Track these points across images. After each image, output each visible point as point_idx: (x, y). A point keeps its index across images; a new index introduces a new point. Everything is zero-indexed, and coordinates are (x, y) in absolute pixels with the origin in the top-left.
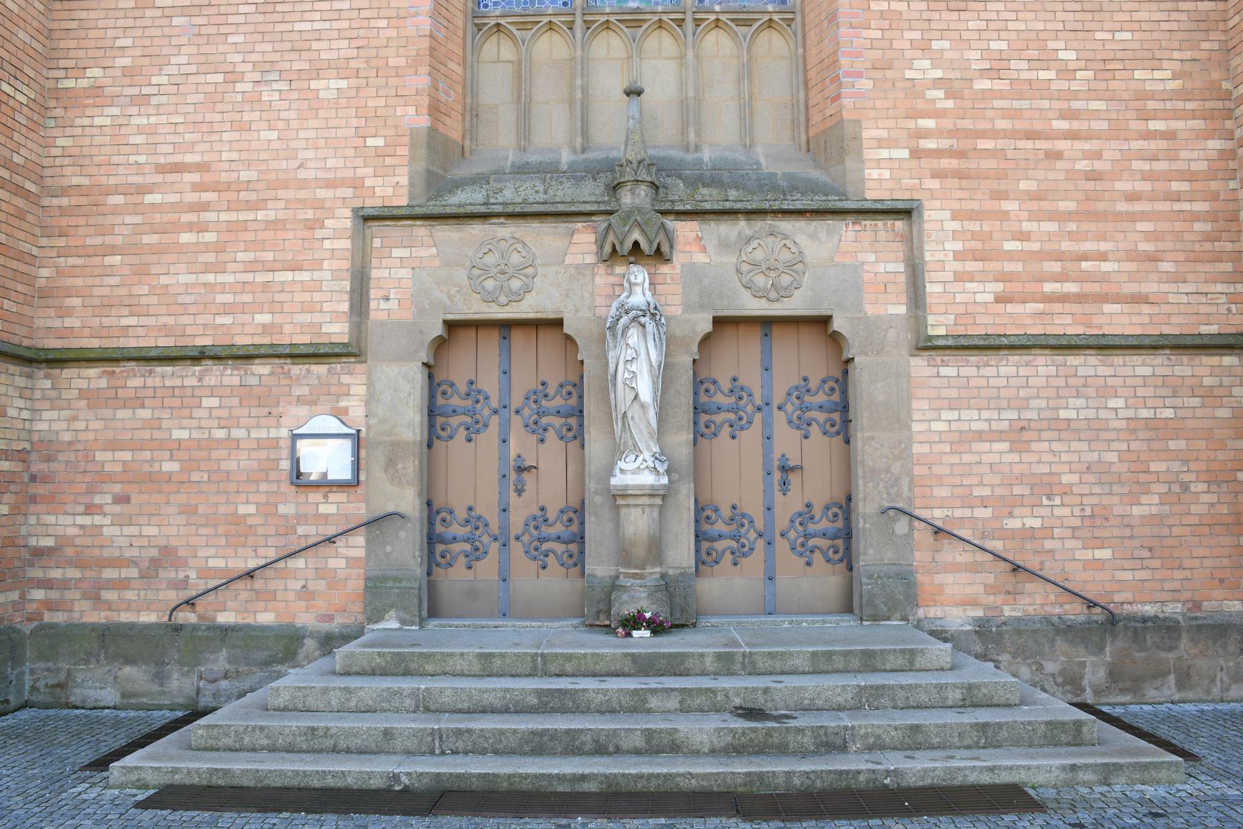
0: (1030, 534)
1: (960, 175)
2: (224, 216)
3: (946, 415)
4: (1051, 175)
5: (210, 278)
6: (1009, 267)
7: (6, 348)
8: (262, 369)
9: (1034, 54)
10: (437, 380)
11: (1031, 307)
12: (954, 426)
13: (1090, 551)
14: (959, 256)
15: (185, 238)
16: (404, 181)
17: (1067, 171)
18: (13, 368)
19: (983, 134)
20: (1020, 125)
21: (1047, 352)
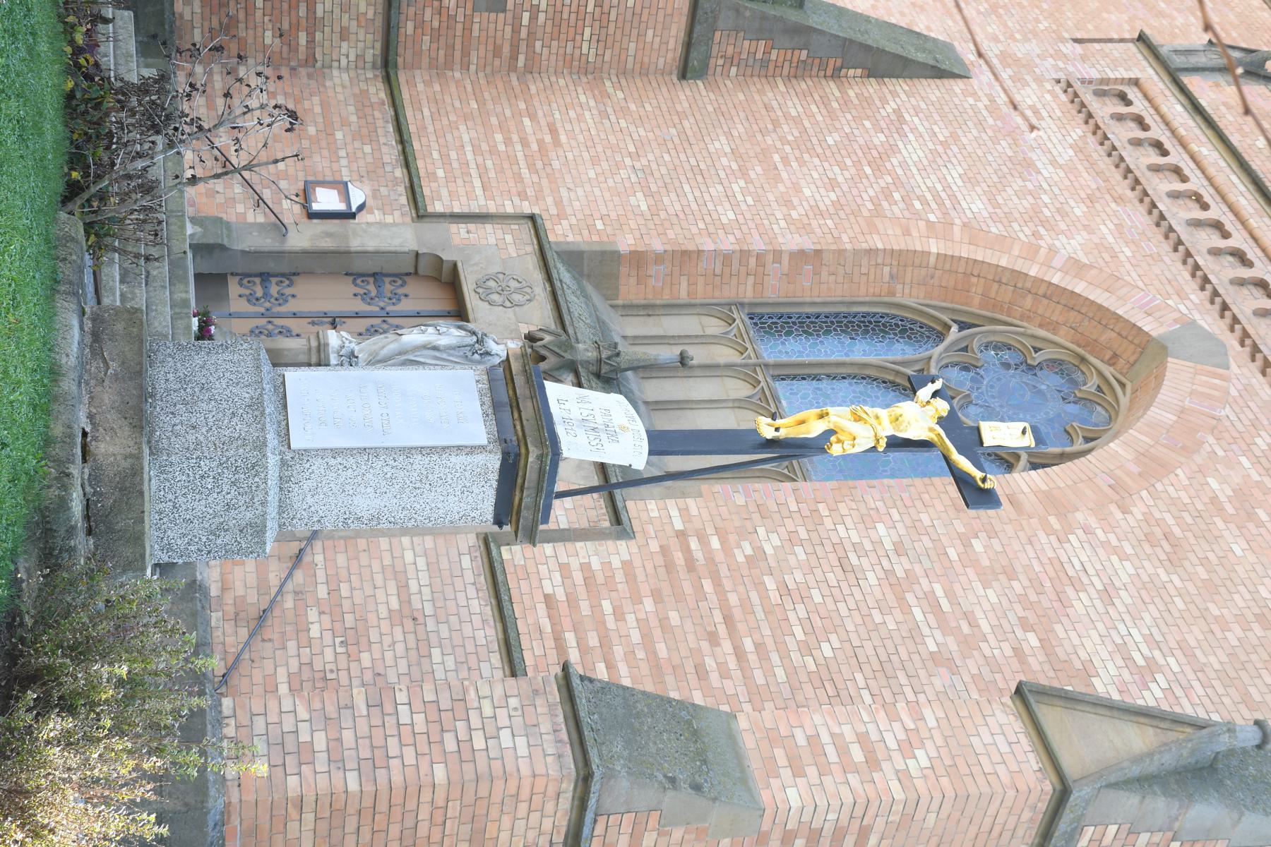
0: (302, 628)
1: (669, 566)
2: (520, 155)
3: (421, 563)
4: (691, 638)
5: (469, 148)
6: (585, 607)
7: (395, 4)
8: (399, 172)
9: (818, 623)
10: (406, 278)
11: (546, 624)
12: (410, 569)
13: (285, 679)
14: (585, 567)
15: (499, 137)
16: (570, 239)
17: (700, 650)
18: (378, 45)
19: (717, 583)
20: (737, 613)
21: (501, 636)
